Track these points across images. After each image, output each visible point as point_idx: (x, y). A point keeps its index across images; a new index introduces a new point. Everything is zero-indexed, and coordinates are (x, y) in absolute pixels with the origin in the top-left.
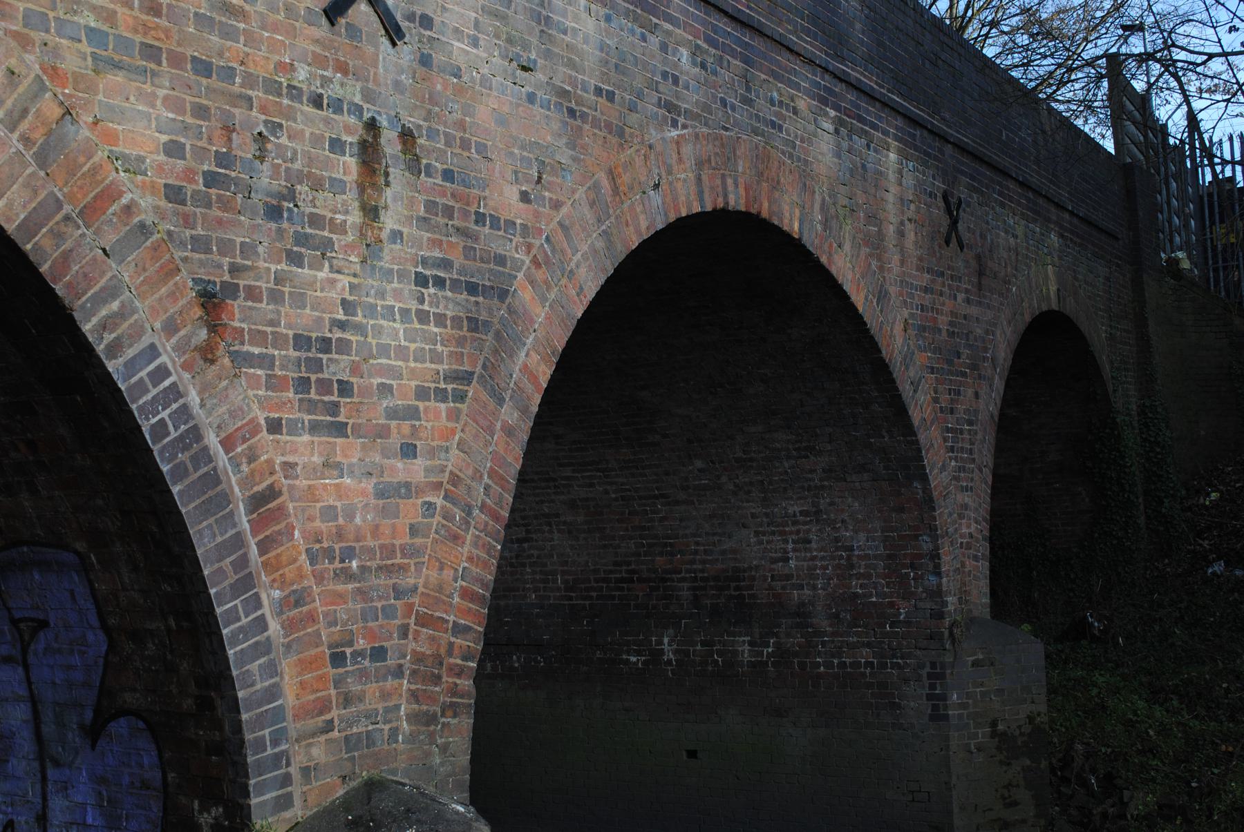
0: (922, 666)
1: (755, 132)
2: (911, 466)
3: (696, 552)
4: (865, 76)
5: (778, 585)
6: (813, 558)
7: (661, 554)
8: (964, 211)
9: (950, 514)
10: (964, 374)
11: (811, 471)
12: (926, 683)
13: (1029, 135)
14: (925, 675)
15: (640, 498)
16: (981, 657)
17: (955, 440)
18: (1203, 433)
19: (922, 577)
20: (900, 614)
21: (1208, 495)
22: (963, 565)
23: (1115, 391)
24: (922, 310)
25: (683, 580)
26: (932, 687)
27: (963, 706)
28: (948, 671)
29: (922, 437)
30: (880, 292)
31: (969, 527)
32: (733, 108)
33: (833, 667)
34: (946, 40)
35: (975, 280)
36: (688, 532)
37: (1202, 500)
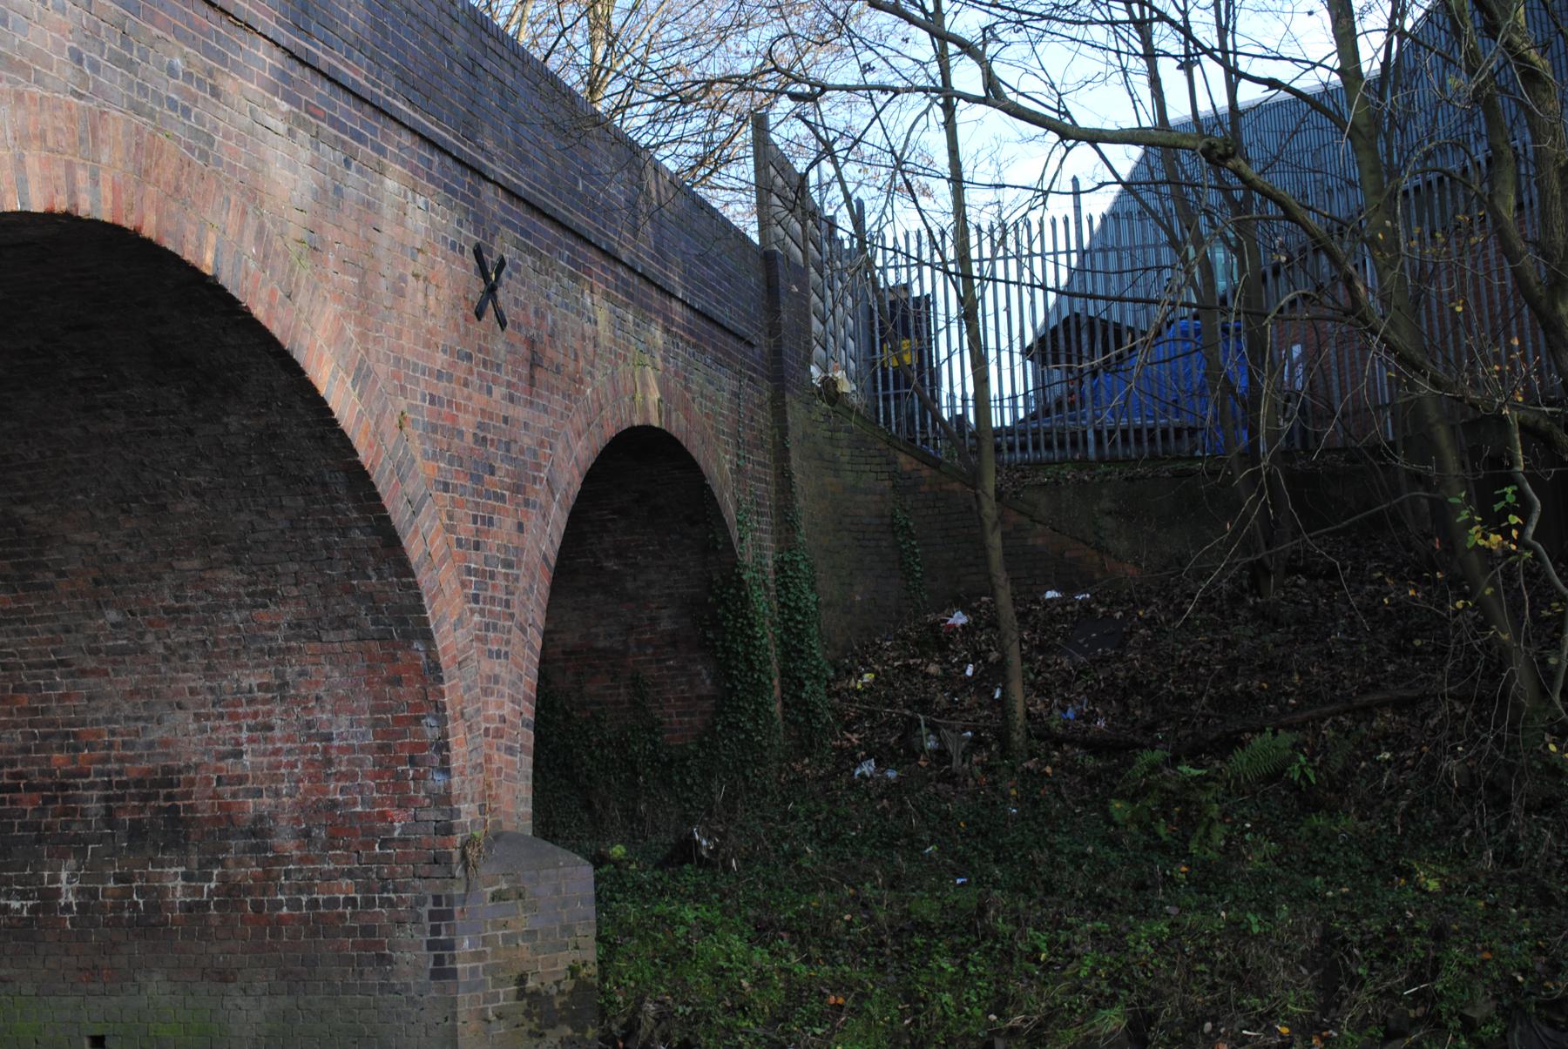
0: (421, 902)
1: (137, 109)
2: (405, 620)
3: (111, 746)
4: (347, 66)
5: (226, 791)
6: (276, 752)
7: (60, 749)
8: (510, 276)
9: (469, 689)
10: (502, 498)
11: (273, 627)
12: (427, 925)
13: (620, 192)
14: (426, 916)
15: (29, 666)
16: (505, 886)
17: (481, 585)
18: (858, 598)
19: (424, 776)
20: (394, 829)
21: (860, 676)
22: (489, 759)
23: (741, 540)
24: (432, 402)
25: (92, 786)
26: (436, 930)
27: (479, 956)
28: (457, 908)
29: (423, 578)
30: (359, 369)
31: (500, 706)
32: (95, 67)
33: (300, 908)
34: (490, 42)
35: (525, 371)
36: (99, 716)
37: (853, 682)
